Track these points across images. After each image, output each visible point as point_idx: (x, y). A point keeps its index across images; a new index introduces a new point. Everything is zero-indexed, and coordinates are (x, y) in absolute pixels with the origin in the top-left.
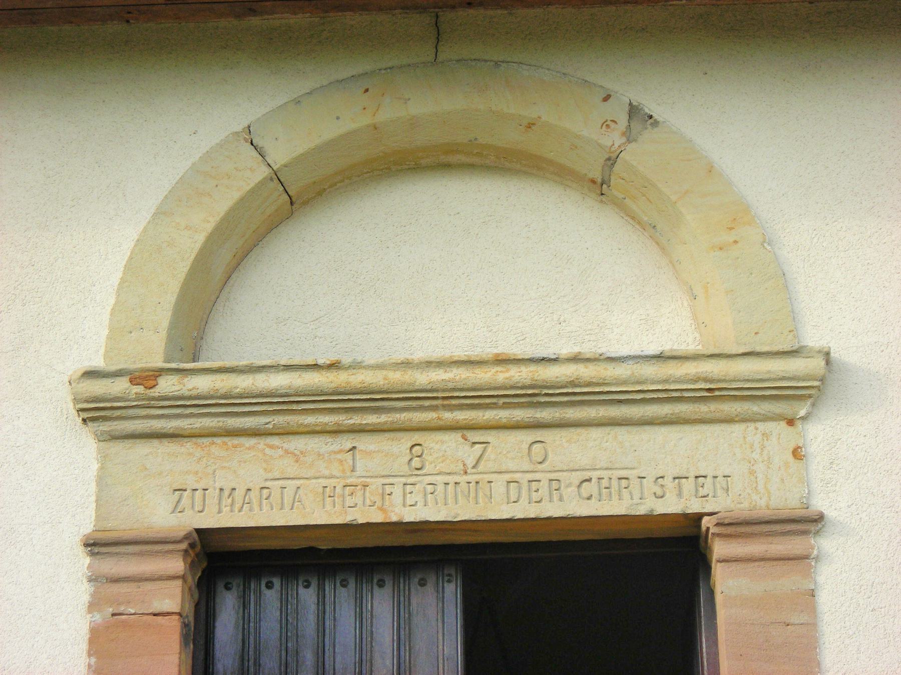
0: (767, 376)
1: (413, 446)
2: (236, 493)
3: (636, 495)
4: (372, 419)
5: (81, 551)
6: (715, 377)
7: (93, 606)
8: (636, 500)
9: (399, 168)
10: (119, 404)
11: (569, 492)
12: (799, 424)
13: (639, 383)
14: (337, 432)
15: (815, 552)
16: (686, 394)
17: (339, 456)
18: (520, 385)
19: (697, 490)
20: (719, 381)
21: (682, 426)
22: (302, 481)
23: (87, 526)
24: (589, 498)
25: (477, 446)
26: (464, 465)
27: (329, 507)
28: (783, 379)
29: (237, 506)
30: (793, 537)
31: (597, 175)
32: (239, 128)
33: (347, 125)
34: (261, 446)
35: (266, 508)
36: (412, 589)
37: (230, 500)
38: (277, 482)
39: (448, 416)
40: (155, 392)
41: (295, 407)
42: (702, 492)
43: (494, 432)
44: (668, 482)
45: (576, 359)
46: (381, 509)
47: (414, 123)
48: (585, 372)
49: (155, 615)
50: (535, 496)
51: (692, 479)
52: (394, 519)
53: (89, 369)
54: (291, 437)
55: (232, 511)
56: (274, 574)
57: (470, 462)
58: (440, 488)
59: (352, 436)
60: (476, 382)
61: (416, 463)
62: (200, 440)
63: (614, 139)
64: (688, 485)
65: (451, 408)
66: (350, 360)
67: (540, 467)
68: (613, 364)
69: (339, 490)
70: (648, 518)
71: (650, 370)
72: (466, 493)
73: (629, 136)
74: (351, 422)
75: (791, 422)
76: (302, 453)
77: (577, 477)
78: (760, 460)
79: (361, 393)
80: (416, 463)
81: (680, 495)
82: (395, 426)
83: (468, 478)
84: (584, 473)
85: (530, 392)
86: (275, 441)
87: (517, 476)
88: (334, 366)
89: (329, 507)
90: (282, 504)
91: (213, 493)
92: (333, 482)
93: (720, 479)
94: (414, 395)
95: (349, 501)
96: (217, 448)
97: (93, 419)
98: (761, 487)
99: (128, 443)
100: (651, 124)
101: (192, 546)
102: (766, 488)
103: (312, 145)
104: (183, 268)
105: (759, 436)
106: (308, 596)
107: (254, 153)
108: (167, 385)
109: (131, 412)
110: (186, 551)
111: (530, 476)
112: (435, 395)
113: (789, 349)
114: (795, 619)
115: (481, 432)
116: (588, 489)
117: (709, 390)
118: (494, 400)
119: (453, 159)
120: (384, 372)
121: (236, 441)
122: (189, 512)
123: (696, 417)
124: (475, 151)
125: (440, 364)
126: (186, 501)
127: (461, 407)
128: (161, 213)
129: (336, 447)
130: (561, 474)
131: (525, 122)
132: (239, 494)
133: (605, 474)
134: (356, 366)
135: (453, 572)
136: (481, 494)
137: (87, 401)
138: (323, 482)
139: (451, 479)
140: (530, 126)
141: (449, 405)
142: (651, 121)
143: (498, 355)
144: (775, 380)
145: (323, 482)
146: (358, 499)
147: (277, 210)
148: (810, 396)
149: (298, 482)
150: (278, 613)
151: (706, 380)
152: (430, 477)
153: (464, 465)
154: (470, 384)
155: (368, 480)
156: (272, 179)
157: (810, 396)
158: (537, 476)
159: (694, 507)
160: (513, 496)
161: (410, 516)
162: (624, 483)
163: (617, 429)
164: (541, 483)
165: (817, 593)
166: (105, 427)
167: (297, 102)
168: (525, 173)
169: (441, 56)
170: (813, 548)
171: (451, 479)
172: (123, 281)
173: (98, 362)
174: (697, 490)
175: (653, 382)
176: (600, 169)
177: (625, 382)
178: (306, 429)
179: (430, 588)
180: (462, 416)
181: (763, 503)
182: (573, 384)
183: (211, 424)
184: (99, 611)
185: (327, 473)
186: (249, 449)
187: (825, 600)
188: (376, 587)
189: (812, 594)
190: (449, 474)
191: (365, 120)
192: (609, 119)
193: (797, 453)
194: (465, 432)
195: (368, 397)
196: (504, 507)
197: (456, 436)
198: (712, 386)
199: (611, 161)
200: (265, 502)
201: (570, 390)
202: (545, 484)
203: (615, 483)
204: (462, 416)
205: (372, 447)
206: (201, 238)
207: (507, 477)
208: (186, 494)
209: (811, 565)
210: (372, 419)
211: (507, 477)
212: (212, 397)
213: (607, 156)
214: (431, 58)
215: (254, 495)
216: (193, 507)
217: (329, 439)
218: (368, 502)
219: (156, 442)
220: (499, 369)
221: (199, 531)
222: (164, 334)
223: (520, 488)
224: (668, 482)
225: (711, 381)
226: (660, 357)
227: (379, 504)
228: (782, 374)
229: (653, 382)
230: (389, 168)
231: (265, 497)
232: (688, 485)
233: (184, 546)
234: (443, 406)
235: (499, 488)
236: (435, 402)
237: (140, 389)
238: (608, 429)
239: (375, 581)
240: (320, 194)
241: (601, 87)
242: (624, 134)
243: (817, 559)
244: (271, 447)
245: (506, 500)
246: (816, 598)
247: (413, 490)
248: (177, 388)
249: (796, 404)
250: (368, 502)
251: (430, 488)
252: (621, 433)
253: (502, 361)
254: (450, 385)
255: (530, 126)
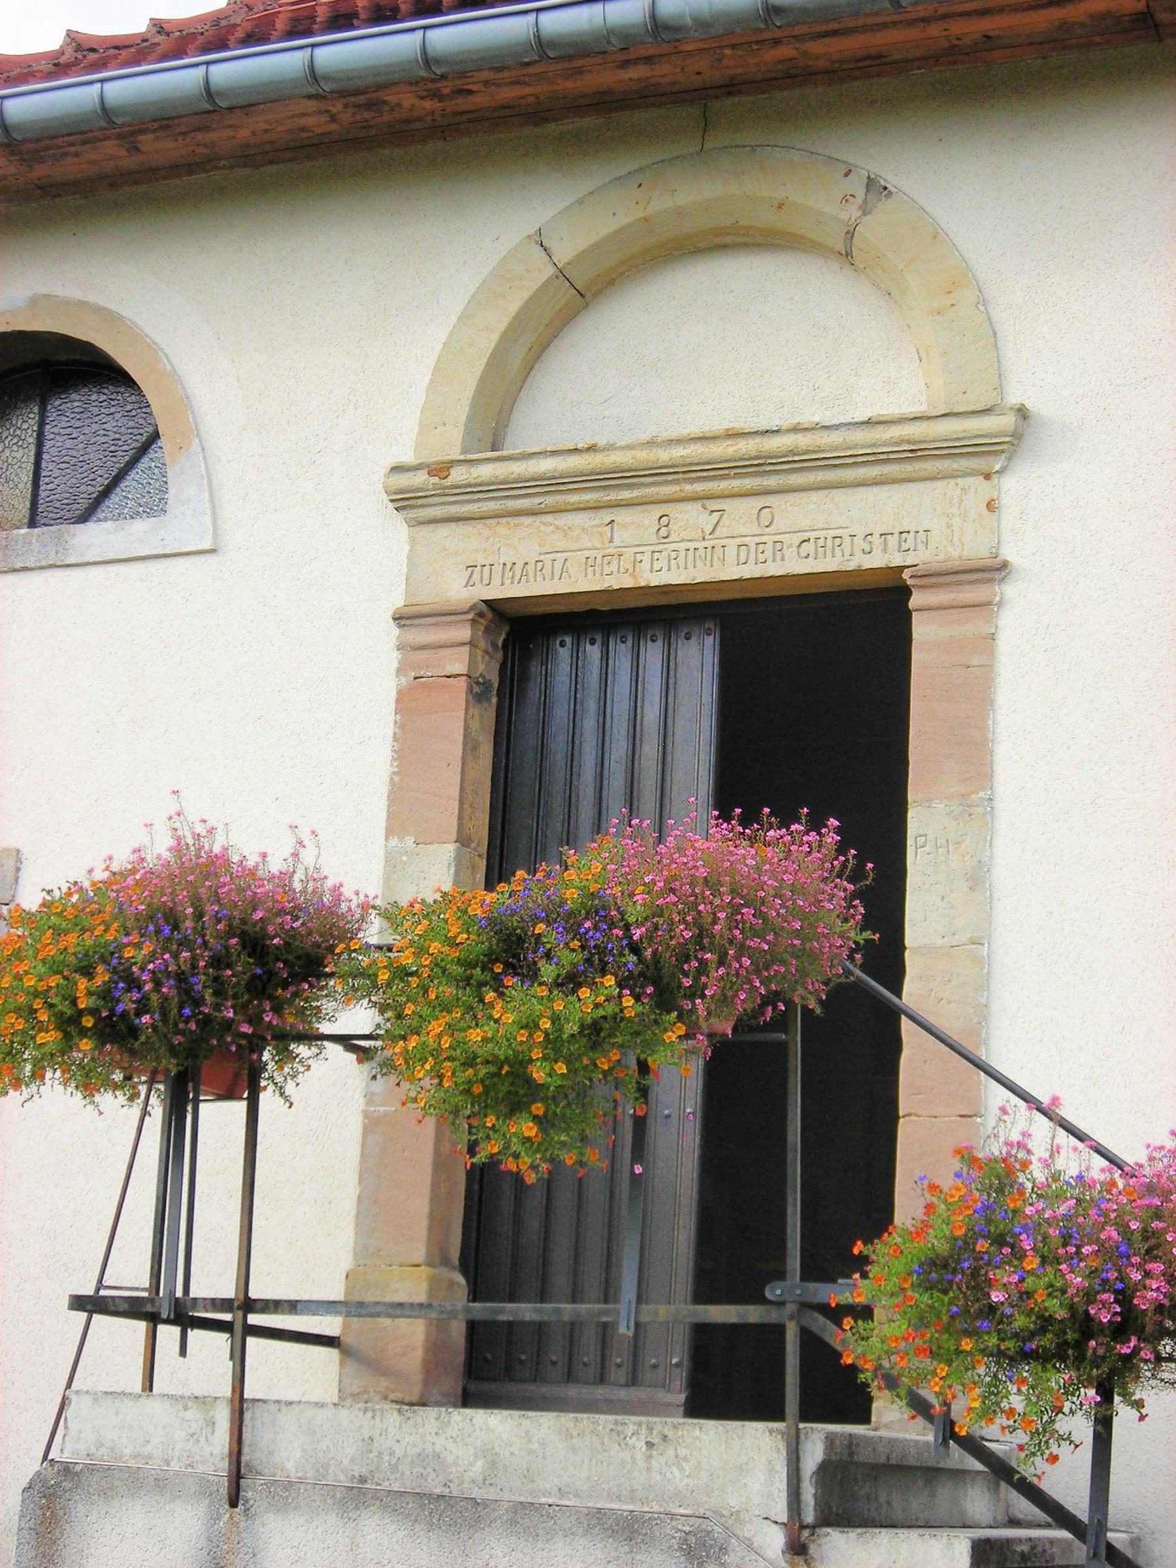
0: (961, 435)
1: (661, 517)
2: (516, 567)
3: (847, 552)
4: (625, 495)
5: (392, 623)
6: (917, 439)
7: (399, 671)
8: (847, 557)
9: (681, 252)
10: (420, 494)
11: (790, 552)
12: (995, 478)
13: (850, 448)
14: (597, 508)
15: (997, 599)
16: (892, 456)
17: (600, 529)
18: (747, 457)
19: (900, 545)
20: (920, 442)
21: (891, 485)
22: (569, 554)
23: (398, 600)
24: (807, 557)
25: (715, 513)
26: (703, 532)
27: (590, 576)
28: (977, 436)
29: (517, 578)
30: (980, 586)
31: (840, 247)
32: (531, 232)
33: (623, 220)
34: (537, 524)
35: (539, 579)
36: (679, 643)
37: (511, 573)
38: (548, 556)
39: (689, 488)
40: (448, 482)
41: (561, 488)
42: (905, 546)
43: (729, 500)
44: (876, 539)
45: (796, 429)
46: (632, 575)
47: (680, 212)
48: (803, 441)
49: (448, 677)
50: (761, 558)
51: (896, 535)
52: (643, 584)
53: (395, 465)
54: (561, 515)
55: (512, 583)
56: (566, 633)
57: (708, 529)
58: (683, 553)
59: (611, 510)
60: (710, 456)
61: (663, 532)
62: (488, 521)
63: (852, 212)
64: (893, 541)
65: (692, 481)
66: (605, 443)
67: (767, 530)
68: (828, 432)
69: (599, 560)
70: (858, 572)
71: (860, 436)
72: (703, 558)
73: (865, 210)
74: (609, 498)
75: (987, 477)
76: (570, 528)
77: (797, 538)
78: (958, 513)
79: (615, 472)
80: (663, 532)
81: (885, 550)
82: (644, 499)
83: (705, 544)
84: (804, 534)
85: (756, 462)
86: (548, 518)
87: (746, 540)
88: (592, 449)
89: (590, 576)
90: (553, 573)
91: (497, 568)
92: (592, 553)
93: (921, 533)
94: (659, 471)
95: (607, 570)
96: (502, 528)
97: (403, 508)
98: (956, 540)
99: (432, 527)
100: (886, 196)
101: (481, 615)
102: (960, 541)
103: (591, 242)
104: (480, 366)
105: (958, 491)
106: (593, 652)
107: (543, 254)
108: (458, 475)
109: (430, 500)
110: (473, 620)
111: (758, 540)
112: (676, 470)
113: (984, 408)
114: (975, 661)
115: (719, 500)
116: (808, 548)
117: (912, 451)
118: (726, 472)
119: (729, 239)
120: (634, 452)
121: (516, 520)
122: (478, 586)
123: (903, 476)
124: (742, 232)
125: (679, 441)
126: (476, 576)
127: (699, 479)
128: (465, 317)
129: (597, 522)
130: (783, 536)
131: (776, 204)
132: (518, 569)
133: (821, 534)
134: (610, 448)
135: (712, 626)
136: (716, 558)
137: (396, 493)
138: (586, 553)
139: (691, 545)
140: (781, 206)
141: (688, 479)
142: (886, 192)
143: (728, 430)
144: (970, 438)
145: (586, 553)
146: (614, 567)
147: (566, 305)
148: (1003, 451)
149: (565, 554)
150: (569, 668)
151: (909, 442)
152: (674, 545)
153: (703, 532)
154: (704, 458)
155: (623, 550)
156: (557, 277)
157: (1003, 451)
158: (764, 539)
159: (897, 561)
160: (743, 559)
161: (655, 580)
162: (838, 541)
163: (835, 492)
164: (767, 546)
165: (998, 636)
166: (414, 514)
167: (580, 202)
168: (792, 248)
169: (707, 146)
170: (995, 596)
171: (691, 545)
172: (432, 381)
173: (409, 458)
174: (900, 545)
175: (863, 447)
176: (842, 242)
177: (836, 449)
178: (572, 507)
179: (693, 641)
180: (699, 487)
181: (956, 554)
182: (792, 452)
183: (496, 507)
184: (405, 675)
185: (589, 545)
186: (527, 527)
187: (1004, 644)
188: (649, 642)
189: (993, 637)
190: (690, 540)
191: (639, 214)
192: (848, 193)
193: (991, 506)
194: (705, 502)
195: (621, 475)
196: (735, 568)
197: (697, 505)
198: (913, 448)
199: (850, 235)
200: (538, 573)
201: (790, 459)
202: (770, 546)
203: (829, 541)
204: (699, 487)
205: (628, 520)
206: (495, 337)
207: (739, 541)
208: (476, 569)
209: (993, 610)
210: (625, 495)
211: (739, 541)
212: (493, 484)
213: (846, 230)
214: (698, 149)
215: (530, 567)
216: (481, 582)
217: (592, 514)
218: (622, 570)
219: (453, 525)
220: (730, 442)
221: (486, 602)
222: (462, 428)
223: (749, 551)
224: (876, 539)
225: (914, 443)
226: (868, 423)
227: (631, 570)
228: (976, 433)
229: (863, 447)
230: (671, 254)
231: (539, 569)
232: (893, 541)
233: (470, 616)
234: (685, 479)
235: (731, 552)
236: (676, 477)
237: (436, 480)
238: (826, 492)
239: (649, 637)
240: (611, 283)
241: (844, 162)
242: (860, 207)
243: (1000, 604)
244: (545, 524)
245: (736, 563)
246: (997, 641)
247: (642, 558)
248: (463, 477)
249: (991, 459)
250: (622, 570)
251: (674, 555)
252: (839, 495)
253: (733, 435)
254: (688, 461)
255: (781, 206)
